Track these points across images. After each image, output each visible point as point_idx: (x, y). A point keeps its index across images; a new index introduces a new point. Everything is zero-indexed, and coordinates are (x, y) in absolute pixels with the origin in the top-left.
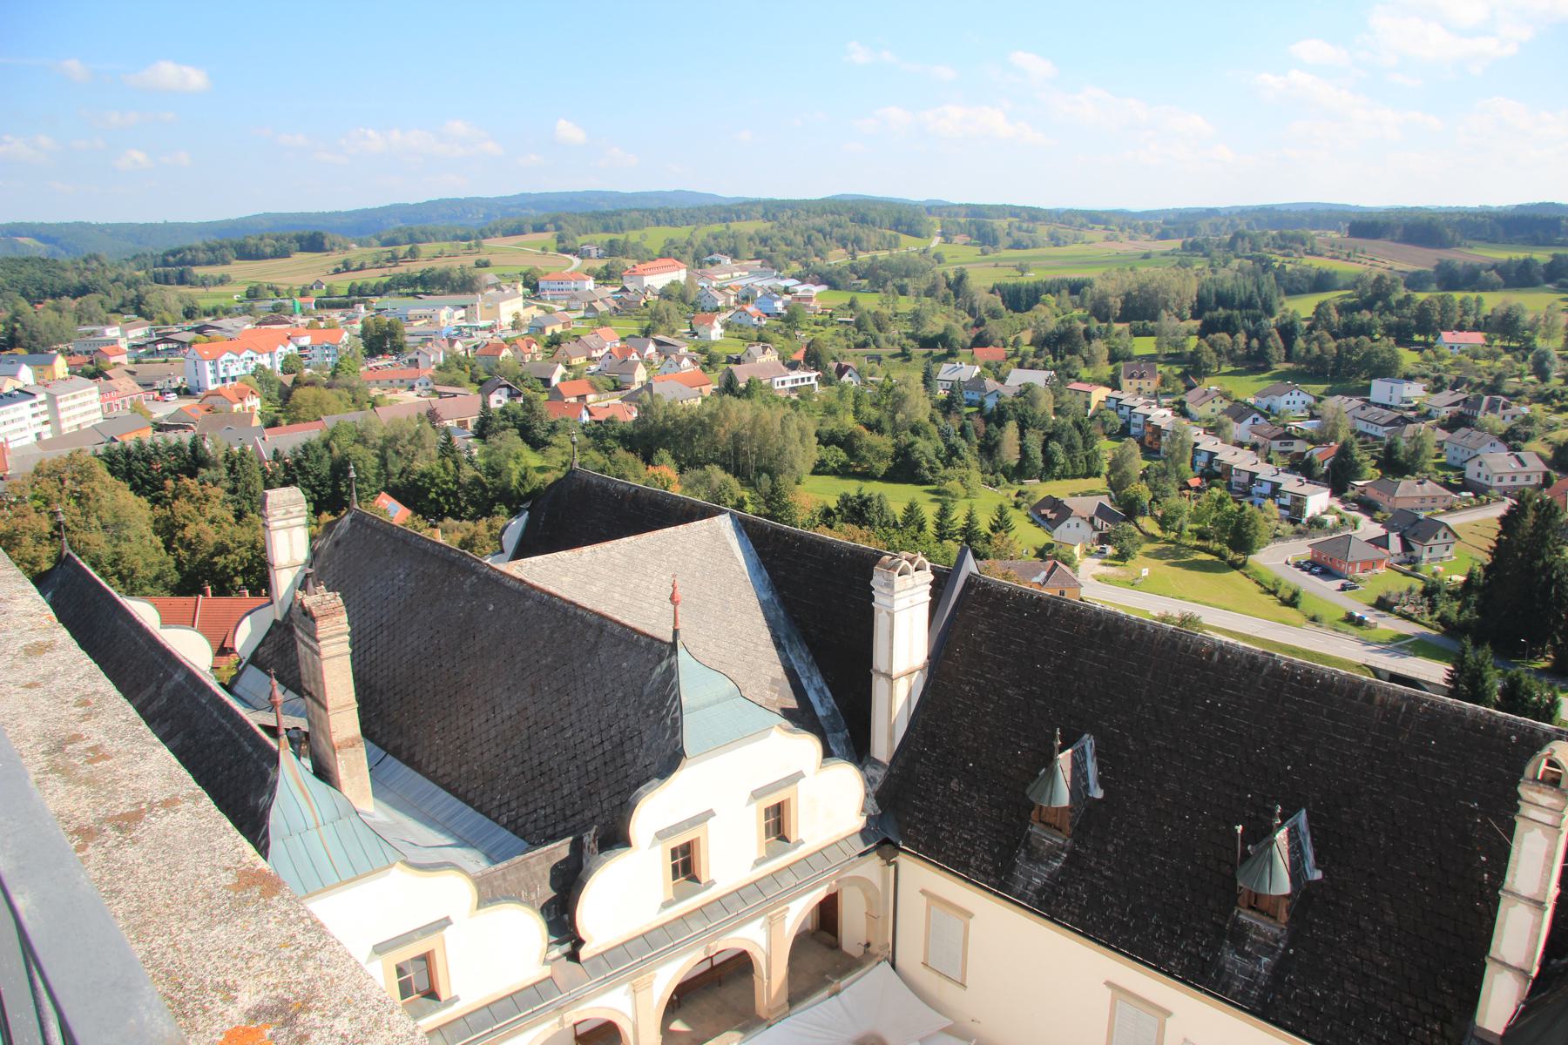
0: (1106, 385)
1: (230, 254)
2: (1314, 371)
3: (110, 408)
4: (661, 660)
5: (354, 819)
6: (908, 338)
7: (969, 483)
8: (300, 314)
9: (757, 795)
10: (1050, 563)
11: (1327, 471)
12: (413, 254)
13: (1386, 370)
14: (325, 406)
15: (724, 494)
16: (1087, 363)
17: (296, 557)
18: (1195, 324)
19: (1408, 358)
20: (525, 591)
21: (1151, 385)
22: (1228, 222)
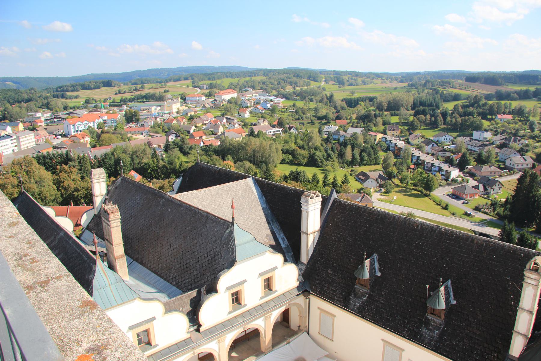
0: (382, 133)
1: (79, 88)
2: (453, 128)
3: (38, 141)
4: (228, 228)
5: (122, 283)
6: (313, 117)
7: (334, 167)
8: (103, 109)
9: (261, 275)
10: (362, 194)
11: (458, 163)
12: (142, 88)
13: (478, 128)
14: (112, 140)
15: (250, 171)
16: (375, 125)
17: (102, 192)
18: (412, 112)
19: (486, 124)
20: (181, 204)
21: (397, 133)
22: (424, 77)
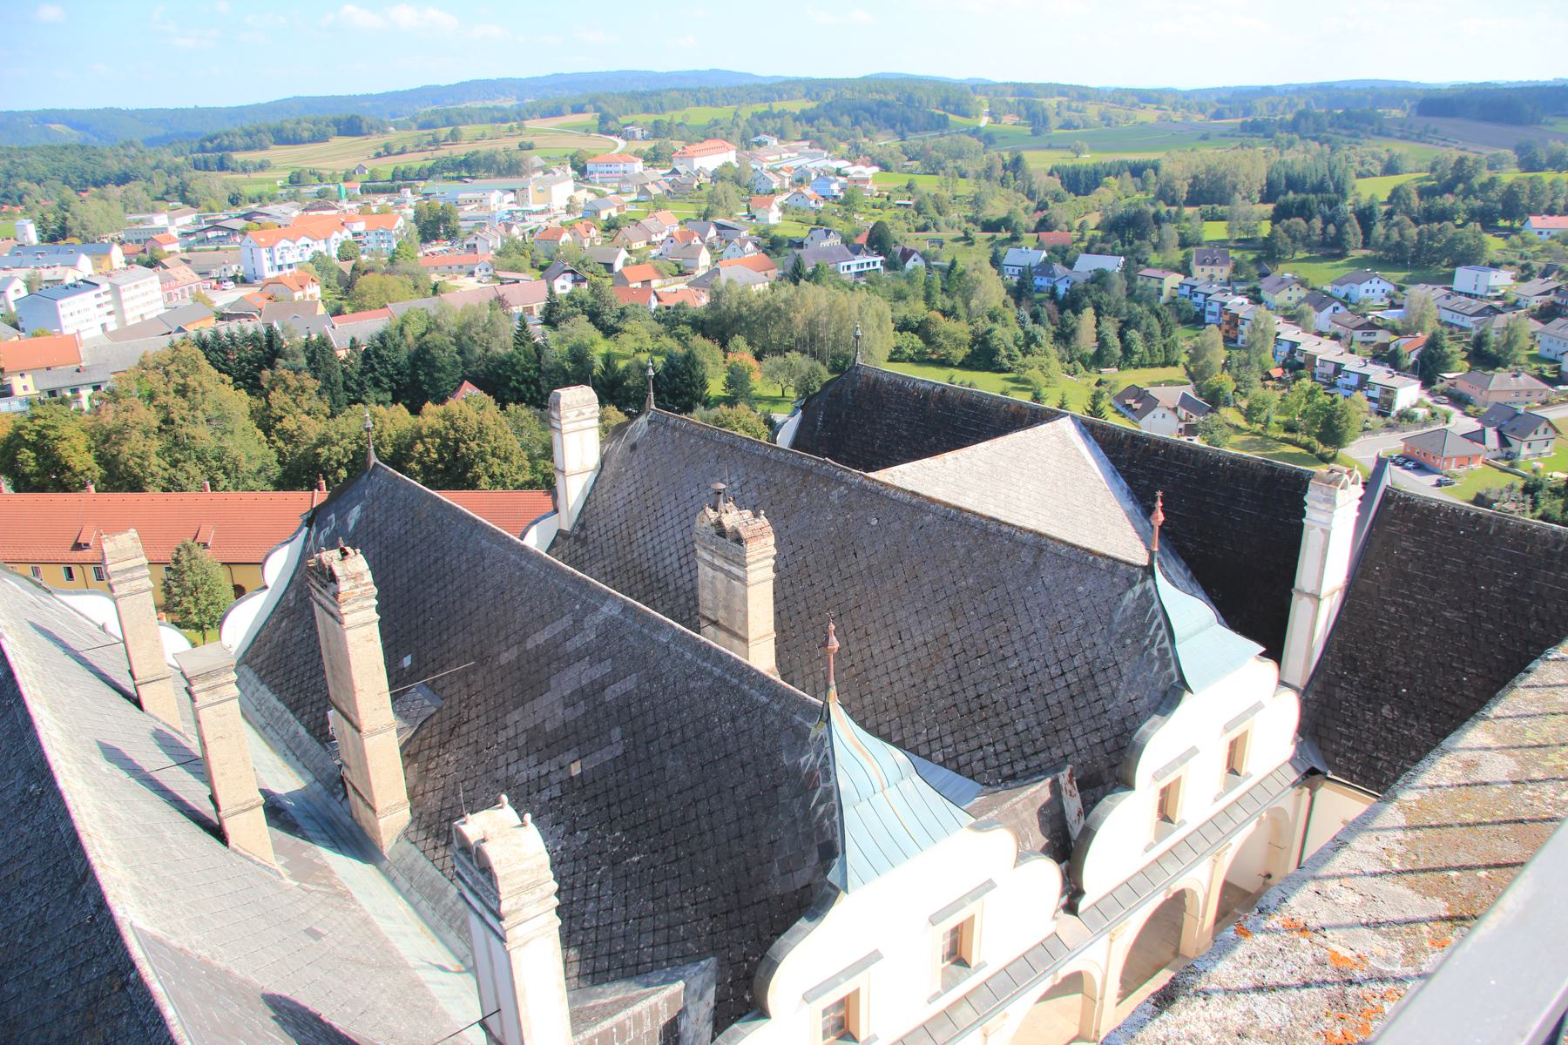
0: (1178, 271)
1: (267, 139)
2: (1395, 257)
3: (170, 297)
4: (1131, 584)
6: (968, 222)
7: (1050, 371)
8: (346, 200)
11: (1415, 362)
12: (455, 137)
13: (1469, 257)
14: (390, 292)
16: (1156, 248)
18: (1269, 208)
19: (1494, 245)
20: (919, 505)
21: (1222, 272)
22: (1286, 101)
